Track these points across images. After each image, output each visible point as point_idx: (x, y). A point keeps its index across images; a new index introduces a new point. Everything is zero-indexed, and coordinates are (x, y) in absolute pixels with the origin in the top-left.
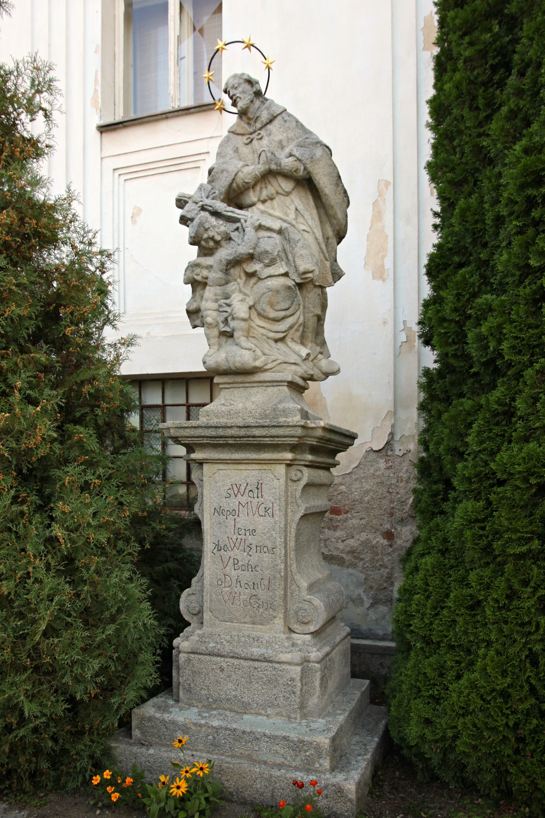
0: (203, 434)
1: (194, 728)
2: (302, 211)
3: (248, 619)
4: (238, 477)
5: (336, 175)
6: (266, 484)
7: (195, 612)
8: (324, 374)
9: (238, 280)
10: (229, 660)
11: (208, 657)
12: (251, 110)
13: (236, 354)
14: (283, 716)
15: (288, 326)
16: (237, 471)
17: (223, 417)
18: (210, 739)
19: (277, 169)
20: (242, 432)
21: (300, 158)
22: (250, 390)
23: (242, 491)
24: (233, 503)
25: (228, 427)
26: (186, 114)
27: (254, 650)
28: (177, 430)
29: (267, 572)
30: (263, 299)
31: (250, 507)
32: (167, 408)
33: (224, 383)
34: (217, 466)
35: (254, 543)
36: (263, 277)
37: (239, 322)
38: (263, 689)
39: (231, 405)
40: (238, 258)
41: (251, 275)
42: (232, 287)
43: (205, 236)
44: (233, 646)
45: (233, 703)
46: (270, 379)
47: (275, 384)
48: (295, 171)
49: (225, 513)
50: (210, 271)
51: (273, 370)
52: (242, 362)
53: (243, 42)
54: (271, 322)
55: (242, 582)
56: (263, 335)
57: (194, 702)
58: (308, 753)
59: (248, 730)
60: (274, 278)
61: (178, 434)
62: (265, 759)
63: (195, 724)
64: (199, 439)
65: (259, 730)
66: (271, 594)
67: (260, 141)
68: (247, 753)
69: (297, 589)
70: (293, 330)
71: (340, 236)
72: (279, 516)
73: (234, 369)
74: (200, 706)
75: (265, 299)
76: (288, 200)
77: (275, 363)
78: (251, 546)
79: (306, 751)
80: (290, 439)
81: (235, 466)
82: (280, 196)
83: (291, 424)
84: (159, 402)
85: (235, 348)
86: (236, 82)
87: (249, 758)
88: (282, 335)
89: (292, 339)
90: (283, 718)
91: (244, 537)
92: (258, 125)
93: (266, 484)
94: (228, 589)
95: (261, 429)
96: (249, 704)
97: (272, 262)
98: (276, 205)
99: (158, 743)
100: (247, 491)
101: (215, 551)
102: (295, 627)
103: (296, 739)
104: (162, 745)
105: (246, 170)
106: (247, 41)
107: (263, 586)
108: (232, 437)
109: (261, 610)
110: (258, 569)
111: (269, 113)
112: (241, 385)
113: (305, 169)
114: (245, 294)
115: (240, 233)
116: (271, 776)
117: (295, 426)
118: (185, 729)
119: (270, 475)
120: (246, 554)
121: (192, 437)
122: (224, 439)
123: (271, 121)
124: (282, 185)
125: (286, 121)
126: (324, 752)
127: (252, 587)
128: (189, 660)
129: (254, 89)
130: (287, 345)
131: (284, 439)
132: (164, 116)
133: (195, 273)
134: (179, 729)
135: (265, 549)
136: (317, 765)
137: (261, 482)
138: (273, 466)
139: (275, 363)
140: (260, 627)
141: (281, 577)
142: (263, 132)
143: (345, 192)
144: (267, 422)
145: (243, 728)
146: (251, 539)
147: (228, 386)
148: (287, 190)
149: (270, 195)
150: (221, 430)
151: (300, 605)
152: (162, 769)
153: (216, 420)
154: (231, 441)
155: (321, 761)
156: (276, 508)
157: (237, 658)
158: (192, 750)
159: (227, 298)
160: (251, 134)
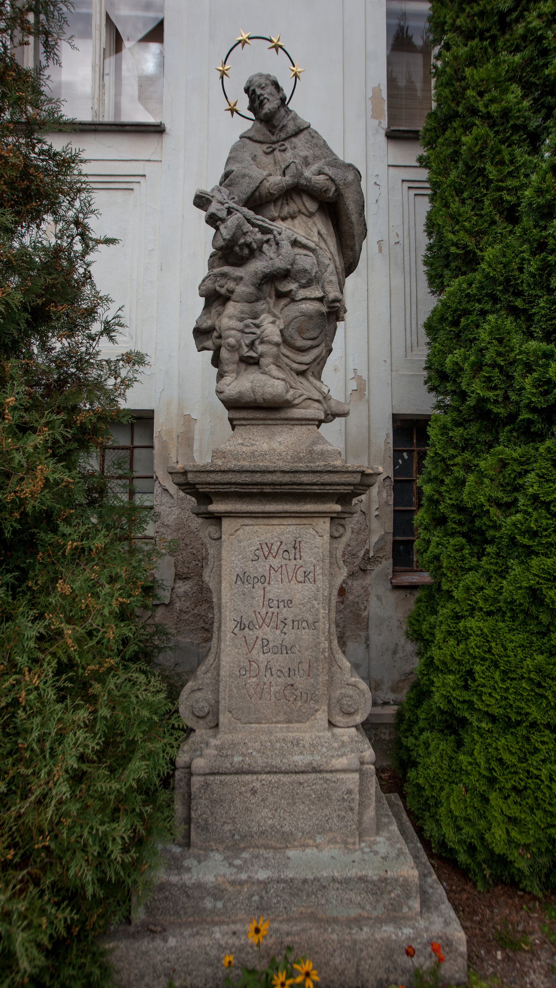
0: (233, 481)
1: (230, 889)
2: (325, 236)
3: (281, 718)
4: (269, 535)
6: (306, 543)
7: (201, 714)
8: (332, 415)
9: (268, 299)
10: (264, 776)
11: (235, 778)
13: (266, 384)
14: (336, 842)
15: (313, 358)
17: (244, 459)
18: (255, 901)
19: (306, 186)
20: (287, 478)
22: (273, 428)
23: (274, 552)
24: (262, 567)
25: (270, 472)
27: (296, 758)
28: (198, 474)
29: (306, 653)
31: (284, 572)
33: (240, 419)
35: (290, 617)
37: (271, 347)
38: (310, 810)
39: (253, 445)
41: (280, 295)
42: (261, 306)
43: (242, 241)
44: (267, 757)
45: (269, 837)
47: (304, 422)
49: (251, 581)
50: (237, 284)
55: (273, 670)
56: (287, 365)
57: (213, 844)
58: (393, 895)
59: (310, 877)
61: (198, 480)
62: (335, 914)
63: (233, 883)
65: (325, 874)
66: (312, 681)
67: (283, 154)
68: (309, 911)
69: (339, 670)
71: (350, 267)
72: (322, 582)
73: (262, 401)
74: (221, 849)
76: (310, 223)
78: (287, 621)
79: (390, 892)
81: (266, 521)
83: (350, 469)
85: (263, 377)
86: (263, 81)
87: (313, 918)
88: (304, 367)
90: (337, 846)
91: (276, 610)
92: (283, 135)
93: (306, 543)
94: (254, 680)
96: (292, 834)
99: (174, 923)
100: (281, 551)
101: (237, 630)
102: (339, 719)
103: (375, 878)
104: (180, 926)
106: (275, 40)
107: (302, 672)
108: (270, 484)
109: (299, 703)
110: (295, 650)
111: (295, 125)
112: (261, 422)
113: (336, 190)
115: (271, 246)
116: (355, 942)
118: (217, 893)
120: (278, 632)
121: (217, 484)
124: (306, 204)
126: (414, 889)
127: (287, 674)
128: (207, 785)
131: (338, 487)
132: (93, 127)
134: (209, 894)
135: (304, 624)
136: (405, 910)
138: (315, 520)
140: (297, 725)
141: (325, 658)
142: (287, 144)
144: (301, 466)
145: (302, 876)
146: (285, 612)
147: (244, 422)
148: (311, 210)
149: (291, 212)
150: (258, 475)
151: (343, 691)
152: (191, 967)
153: (234, 462)
154: (268, 490)
155: (411, 903)
156: (319, 571)
157: (275, 773)
158: (228, 924)
159: (255, 318)
160: (274, 143)
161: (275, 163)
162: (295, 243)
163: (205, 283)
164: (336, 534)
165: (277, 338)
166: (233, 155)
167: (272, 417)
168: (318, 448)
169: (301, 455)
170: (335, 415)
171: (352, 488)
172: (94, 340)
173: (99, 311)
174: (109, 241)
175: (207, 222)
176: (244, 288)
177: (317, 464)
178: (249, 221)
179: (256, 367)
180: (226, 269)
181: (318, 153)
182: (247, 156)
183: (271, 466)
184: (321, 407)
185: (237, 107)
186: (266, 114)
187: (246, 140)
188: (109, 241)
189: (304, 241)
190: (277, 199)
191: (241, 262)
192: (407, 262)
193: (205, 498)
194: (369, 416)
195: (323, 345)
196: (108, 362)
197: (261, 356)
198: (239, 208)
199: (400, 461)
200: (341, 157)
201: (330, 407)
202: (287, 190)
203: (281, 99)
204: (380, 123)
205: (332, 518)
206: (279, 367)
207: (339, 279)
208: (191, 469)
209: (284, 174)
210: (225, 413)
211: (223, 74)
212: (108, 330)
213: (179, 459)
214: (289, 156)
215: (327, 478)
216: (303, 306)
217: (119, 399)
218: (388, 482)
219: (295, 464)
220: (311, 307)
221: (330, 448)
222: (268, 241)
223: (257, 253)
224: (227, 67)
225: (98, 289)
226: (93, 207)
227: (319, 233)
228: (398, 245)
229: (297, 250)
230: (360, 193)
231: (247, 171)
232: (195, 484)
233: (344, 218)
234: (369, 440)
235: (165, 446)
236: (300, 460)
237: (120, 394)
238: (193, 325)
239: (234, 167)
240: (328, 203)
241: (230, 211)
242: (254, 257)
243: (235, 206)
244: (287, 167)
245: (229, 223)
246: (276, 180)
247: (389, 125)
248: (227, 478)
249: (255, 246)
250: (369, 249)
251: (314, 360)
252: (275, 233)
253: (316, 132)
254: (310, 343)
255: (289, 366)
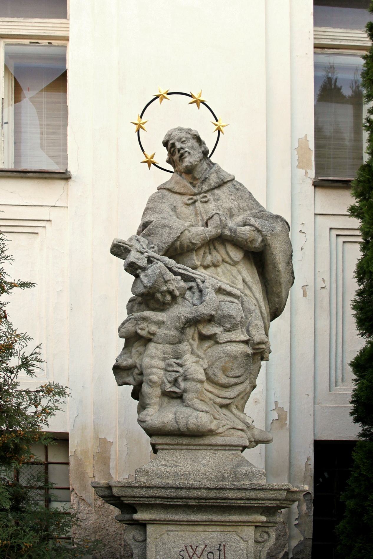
0: (158, 495)
2: (250, 284)
4: (193, 539)
5: (290, 253)
8: (255, 442)
12: (199, 169)
15: (237, 393)
16: (193, 533)
19: (230, 236)
20: (212, 494)
21: (260, 228)
25: (194, 489)
26: (22, 178)
28: (123, 489)
30: (217, 363)
32: (50, 466)
33: (163, 444)
34: (165, 528)
36: (221, 342)
37: (195, 383)
40: (199, 318)
41: (203, 338)
42: (185, 347)
43: (164, 288)
46: (224, 443)
47: (228, 448)
48: (251, 242)
51: (223, 434)
52: (199, 424)
53: (191, 96)
54: (218, 387)
56: (210, 399)
60: (234, 344)
61: (123, 494)
64: (150, 499)
67: (205, 205)
70: (239, 398)
71: (275, 314)
73: (185, 430)
75: (219, 364)
76: (234, 270)
77: (225, 427)
80: (269, 502)
81: (191, 528)
82: (225, 264)
83: (275, 487)
84: (43, 459)
85: (185, 409)
86: (183, 135)
89: (237, 406)
92: (205, 187)
95: (236, 491)
97: (234, 327)
98: (221, 273)
100: (205, 553)
105: (193, 230)
108: (195, 499)
111: (218, 177)
113: (263, 241)
114: (198, 356)
115: (193, 293)
117: (279, 490)
119: (235, 536)
121: (142, 497)
122: (184, 500)
123: (219, 186)
124: (231, 253)
125: (237, 189)
129: (203, 149)
130: (232, 412)
131: (263, 502)
133: (140, 327)
137: (224, 543)
138: (240, 528)
139: (225, 427)
142: (209, 196)
143: (293, 273)
144: (226, 484)
147: (167, 447)
148: (236, 259)
149: (215, 262)
150: (183, 491)
154: (192, 503)
159: (177, 358)
160: (195, 195)
161: (196, 214)
162: (220, 291)
163: (125, 325)
164: (260, 540)
165: (203, 377)
166: (151, 205)
167: (196, 443)
168: (242, 469)
169: (226, 475)
170: (257, 442)
171: (277, 502)
172: (12, 373)
173: (16, 347)
174: (23, 285)
175: (126, 270)
176: (166, 332)
177: (242, 483)
178: (170, 269)
179: (179, 401)
180: (147, 313)
181: (243, 204)
182: (166, 207)
183: (196, 484)
184: (245, 435)
185: (155, 160)
186: (187, 167)
187: (165, 191)
188: (23, 285)
189: (229, 289)
190: (199, 248)
191: (162, 307)
192: (334, 306)
193: (131, 509)
194: (290, 441)
195: (248, 382)
196: (28, 392)
197: (185, 391)
198: (159, 257)
199: (321, 480)
200: (263, 203)
201: (253, 436)
202: (210, 240)
203: (203, 152)
204: (306, 173)
205: (256, 527)
206: (203, 401)
207: (264, 323)
208: (116, 484)
209: (206, 224)
210: (146, 439)
211: (139, 128)
212: (25, 364)
213: (96, 474)
214: (211, 207)
215: (252, 494)
216: (228, 348)
217: (41, 425)
218: (308, 497)
219: (221, 483)
220: (236, 349)
221: (254, 470)
222: (190, 289)
223: (180, 300)
224: (143, 120)
225: (14, 328)
226: (6, 253)
227: (244, 281)
228: (323, 290)
229: (222, 297)
230: (289, 244)
231: (166, 222)
232: (119, 497)
233: (271, 266)
234: (290, 463)
235: (80, 464)
236: (224, 479)
237: (42, 420)
238: (114, 362)
239: (152, 217)
240: (253, 253)
241: (150, 260)
242: (176, 303)
243: (155, 255)
244: (210, 218)
245: (149, 271)
246: (198, 232)
247: (317, 174)
248: (151, 492)
249: (177, 293)
250: (297, 299)
251: (238, 395)
252: (199, 281)
253: (241, 185)
254: (234, 380)
255: (213, 400)
